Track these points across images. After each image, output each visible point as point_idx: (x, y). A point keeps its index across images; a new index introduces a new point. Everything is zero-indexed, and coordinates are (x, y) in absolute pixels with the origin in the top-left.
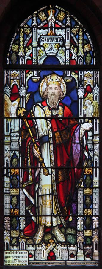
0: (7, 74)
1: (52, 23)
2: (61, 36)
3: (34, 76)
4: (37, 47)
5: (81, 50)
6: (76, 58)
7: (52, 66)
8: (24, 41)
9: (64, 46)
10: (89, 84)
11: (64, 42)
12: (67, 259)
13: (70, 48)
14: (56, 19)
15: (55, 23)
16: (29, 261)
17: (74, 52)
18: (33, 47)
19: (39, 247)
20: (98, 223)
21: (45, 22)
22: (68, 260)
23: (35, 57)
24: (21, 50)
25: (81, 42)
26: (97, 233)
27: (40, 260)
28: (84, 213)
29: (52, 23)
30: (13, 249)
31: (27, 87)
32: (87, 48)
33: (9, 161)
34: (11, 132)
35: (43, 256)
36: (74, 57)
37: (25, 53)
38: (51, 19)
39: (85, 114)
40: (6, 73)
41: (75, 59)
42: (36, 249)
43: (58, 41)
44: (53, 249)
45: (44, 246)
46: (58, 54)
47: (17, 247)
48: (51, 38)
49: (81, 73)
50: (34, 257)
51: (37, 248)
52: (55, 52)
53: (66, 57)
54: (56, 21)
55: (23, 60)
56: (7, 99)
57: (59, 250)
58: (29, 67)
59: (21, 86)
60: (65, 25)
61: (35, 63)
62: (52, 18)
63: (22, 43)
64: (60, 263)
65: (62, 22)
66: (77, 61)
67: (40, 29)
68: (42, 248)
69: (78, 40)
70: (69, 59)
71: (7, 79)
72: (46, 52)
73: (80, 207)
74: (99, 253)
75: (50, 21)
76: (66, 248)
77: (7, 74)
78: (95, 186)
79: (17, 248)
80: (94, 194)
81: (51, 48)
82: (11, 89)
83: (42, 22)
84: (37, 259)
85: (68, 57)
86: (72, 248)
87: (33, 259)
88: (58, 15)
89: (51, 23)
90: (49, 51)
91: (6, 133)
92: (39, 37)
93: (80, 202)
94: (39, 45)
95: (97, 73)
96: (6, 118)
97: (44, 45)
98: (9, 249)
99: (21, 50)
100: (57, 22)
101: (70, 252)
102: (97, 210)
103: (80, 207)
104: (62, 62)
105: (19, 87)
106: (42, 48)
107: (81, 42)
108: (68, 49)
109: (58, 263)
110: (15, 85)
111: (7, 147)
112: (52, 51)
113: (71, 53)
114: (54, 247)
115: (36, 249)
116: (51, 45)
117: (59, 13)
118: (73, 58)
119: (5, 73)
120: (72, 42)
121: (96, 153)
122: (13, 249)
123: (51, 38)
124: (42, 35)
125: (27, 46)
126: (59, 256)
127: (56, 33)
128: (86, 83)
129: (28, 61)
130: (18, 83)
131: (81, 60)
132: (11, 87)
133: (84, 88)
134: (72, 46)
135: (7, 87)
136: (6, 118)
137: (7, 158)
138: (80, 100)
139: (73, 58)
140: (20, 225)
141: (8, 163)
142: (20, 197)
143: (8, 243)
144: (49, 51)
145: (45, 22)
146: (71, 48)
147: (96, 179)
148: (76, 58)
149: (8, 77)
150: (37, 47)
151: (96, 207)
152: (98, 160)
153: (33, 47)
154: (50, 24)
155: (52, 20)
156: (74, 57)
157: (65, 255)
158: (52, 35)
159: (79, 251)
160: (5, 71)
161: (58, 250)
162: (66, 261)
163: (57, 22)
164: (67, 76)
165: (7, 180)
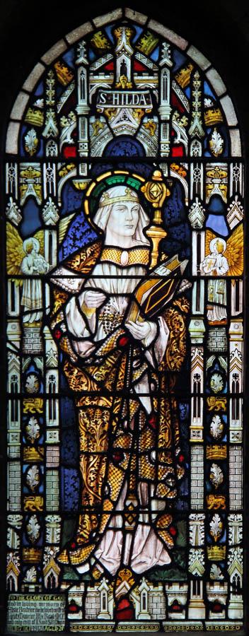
3: (78, 177)
4: (88, 117)
6: (185, 142)
9: (155, 112)
11: (157, 105)
12: (164, 617)
13: (171, 116)
14: (136, 51)
15: (133, 59)
17: (178, 127)
20: (241, 530)
22: (168, 619)
28: (206, 504)
31: (60, 204)
33: (202, 378)
35: (104, 608)
40: (48, 171)
41: (181, 144)
43: (136, 102)
44: (130, 592)
46: (141, 130)
47: (223, 586)
50: (81, 613)
53: (162, 139)
56: (13, 238)
59: (44, 202)
60: (157, 63)
62: (123, 47)
69: (191, 99)
70: (168, 145)
72: (109, 126)
75: (119, 54)
76: (160, 588)
77: (50, 174)
78: (193, 439)
79: (222, 588)
80: (232, 459)
81: (126, 120)
82: (20, 207)
86: (217, 588)
87: (78, 616)
88: (139, 40)
92: (93, 91)
94: (93, 111)
97: (107, 112)
99: (51, 124)
100: (139, 56)
102: (239, 497)
105: (225, 200)
106: (102, 120)
108: (166, 122)
109: (86, 627)
110: (31, 197)
114: (133, 588)
116: (122, 112)
117: (142, 36)
119: (7, 169)
120: (175, 105)
121: (236, 362)
126: (144, 608)
129: (67, 148)
134: (176, 114)
135: (12, 204)
137: (198, 370)
138: (195, 235)
139: (178, 140)
140: (228, 533)
141: (16, 385)
142: (231, 465)
144: (118, 122)
146: (174, 118)
148: (185, 142)
149: (14, 179)
150: (88, 117)
152: (240, 377)
153: (78, 117)
155: (125, 51)
156: (182, 137)
157: (158, 610)
158: (123, 87)
159: (233, 597)
160: (7, 164)
161: (140, 595)
162: (161, 621)
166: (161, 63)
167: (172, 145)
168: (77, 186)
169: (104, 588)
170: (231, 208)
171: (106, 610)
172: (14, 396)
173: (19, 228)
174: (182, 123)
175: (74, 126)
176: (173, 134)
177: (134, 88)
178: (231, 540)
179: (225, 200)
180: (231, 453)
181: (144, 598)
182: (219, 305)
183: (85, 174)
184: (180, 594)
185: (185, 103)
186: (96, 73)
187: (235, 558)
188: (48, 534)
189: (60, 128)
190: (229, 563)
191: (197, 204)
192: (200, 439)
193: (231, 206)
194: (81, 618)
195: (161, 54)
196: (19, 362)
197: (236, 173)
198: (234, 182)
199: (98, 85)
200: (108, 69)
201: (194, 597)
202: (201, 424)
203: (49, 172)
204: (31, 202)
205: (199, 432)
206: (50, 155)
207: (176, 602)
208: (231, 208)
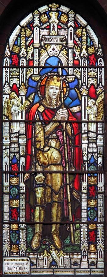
0: (6, 73)
3: (34, 74)
5: (84, 51)
10: (93, 83)
15: (58, 25)
16: (30, 269)
19: (40, 255)
21: (48, 24)
24: (23, 50)
25: (84, 43)
29: (55, 24)
35: (46, 264)
36: (78, 57)
37: (27, 52)
38: (53, 21)
39: (89, 114)
45: (45, 254)
51: (38, 256)
52: (49, 52)
54: (59, 23)
57: (61, 258)
63: (23, 43)
64: (85, 272)
66: (80, 61)
68: (44, 256)
69: (81, 42)
71: (6, 78)
78: (99, 191)
79: (95, 255)
85: (71, 57)
87: (35, 267)
89: (54, 25)
95: (23, 70)
99: (23, 50)
100: (60, 24)
107: (84, 43)
110: (92, 84)
117: (61, 15)
118: (76, 58)
124: (45, 35)
125: (29, 46)
127: (60, 33)
128: (89, 81)
131: (85, 61)
132: (89, 86)
133: (10, 86)
139: (76, 58)
145: (48, 24)
156: (78, 57)
163: (60, 24)
164: (69, 74)
166: (69, 25)
167: (74, 59)
169: (45, 256)
171: (47, 265)
174: (78, 50)
182: (92, 132)
184: (94, 258)
185: (79, 43)
186: (43, 29)
187: (6, 243)
189: (27, 52)
190: (97, 245)
191: (84, 86)
194: (95, 268)
198: (22, 77)
199: (43, 34)
200: (48, 28)
201: (100, 259)
202: (86, 184)
203: (6, 72)
204: (92, 86)
205: (101, 188)
206: (22, 65)
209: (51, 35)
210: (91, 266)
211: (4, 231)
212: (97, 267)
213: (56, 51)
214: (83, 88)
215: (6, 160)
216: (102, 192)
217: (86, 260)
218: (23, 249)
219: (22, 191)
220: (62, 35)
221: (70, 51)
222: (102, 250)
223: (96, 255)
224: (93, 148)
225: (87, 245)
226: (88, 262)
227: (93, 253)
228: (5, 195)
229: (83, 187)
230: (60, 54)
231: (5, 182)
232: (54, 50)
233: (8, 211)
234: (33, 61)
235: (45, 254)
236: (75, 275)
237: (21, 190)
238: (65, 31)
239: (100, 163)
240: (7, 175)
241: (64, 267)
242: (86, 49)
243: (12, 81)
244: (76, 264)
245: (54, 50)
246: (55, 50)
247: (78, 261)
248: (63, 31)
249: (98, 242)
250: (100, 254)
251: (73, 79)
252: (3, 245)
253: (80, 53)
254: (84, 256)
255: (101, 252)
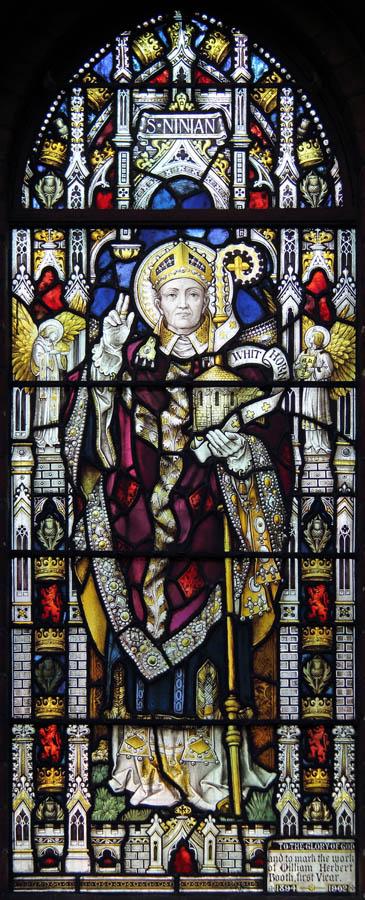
1: (185, 67)
2: (218, 114)
3: (118, 240)
5: (286, 159)
7: (183, 214)
8: (87, 127)
15: (194, 67)
17: (260, 163)
18: (117, 150)
23: (124, 183)
24: (77, 159)
25: (287, 131)
26: (291, 783)
27: (142, 871)
29: (185, 67)
30: (311, 833)
32: (308, 153)
33: (29, 530)
34: (34, 429)
37: (90, 167)
42: (127, 837)
48: (187, 121)
49: (290, 236)
55: (79, 194)
56: (23, 318)
58: (102, 214)
61: (123, 204)
65: (219, 67)
67: (143, 88)
68: (150, 832)
69: (277, 131)
70: (243, 190)
73: (289, 692)
74: (11, 853)
76: (234, 832)
81: (180, 150)
83: (145, 66)
84: (128, 870)
85: (240, 182)
89: (181, 70)
90: (172, 161)
91: (16, 434)
93: (288, 674)
96: (21, 384)
98: (297, 833)
99: (77, 159)
101: (100, 849)
103: (289, 692)
104: (221, 203)
105: (331, 277)
107: (287, 131)
110: (50, 269)
111: (21, 480)
112: (185, 163)
113: (250, 168)
115: (127, 837)
118: (258, 183)
122: (311, 833)
123: (187, 121)
130: (61, 262)
136: (21, 384)
139: (258, 183)
143: (82, 820)
144: (172, 161)
147: (345, 597)
150: (130, 149)
151: (22, 657)
154: (176, 71)
156: (264, 179)
159: (74, 845)
165: (23, 597)
167: (249, 188)
168: (117, 253)
170: (70, 286)
172: (22, 554)
173: (31, 309)
175: (110, 162)
176: (252, 176)
177: (198, 109)
178: (71, 762)
179: (331, 277)
180: (71, 639)
181: (156, 848)
183: (128, 237)
188: (337, 762)
192: (295, 620)
193: (70, 282)
195: (234, 62)
196: (29, 502)
197: (290, 238)
207: (107, 853)
208: (70, 286)
209: (173, 107)
210: (103, 865)
211: (15, 747)
212: (123, 867)
213: (190, 160)
214: (342, 284)
215: (22, 520)
216: (295, 620)
217: (82, 845)
218: (78, 807)
219: (290, 619)
220: (212, 111)
221: (239, 156)
222: (350, 814)
223: (62, 830)
224: (51, 479)
225: (89, 795)
226: (35, 853)
227: (109, 826)
228: (74, 630)
229: (19, 610)
230: (210, 172)
231: (341, 587)
232: (183, 155)
233: (85, 680)
234: (110, 195)
235: (156, 826)
236: (177, 894)
237: (286, 615)
238: (161, 95)
239: (345, 528)
240: (347, 562)
241: (218, 868)
242: (82, 155)
243: (307, 260)
244: (109, 861)
245: (183, 155)
246: (187, 155)
247: (116, 850)
248: (152, 96)
249: (14, 785)
250: (74, 826)
251: (136, 253)
252: (14, 794)
253: (274, 165)
254: (77, 834)
255: (78, 821)
